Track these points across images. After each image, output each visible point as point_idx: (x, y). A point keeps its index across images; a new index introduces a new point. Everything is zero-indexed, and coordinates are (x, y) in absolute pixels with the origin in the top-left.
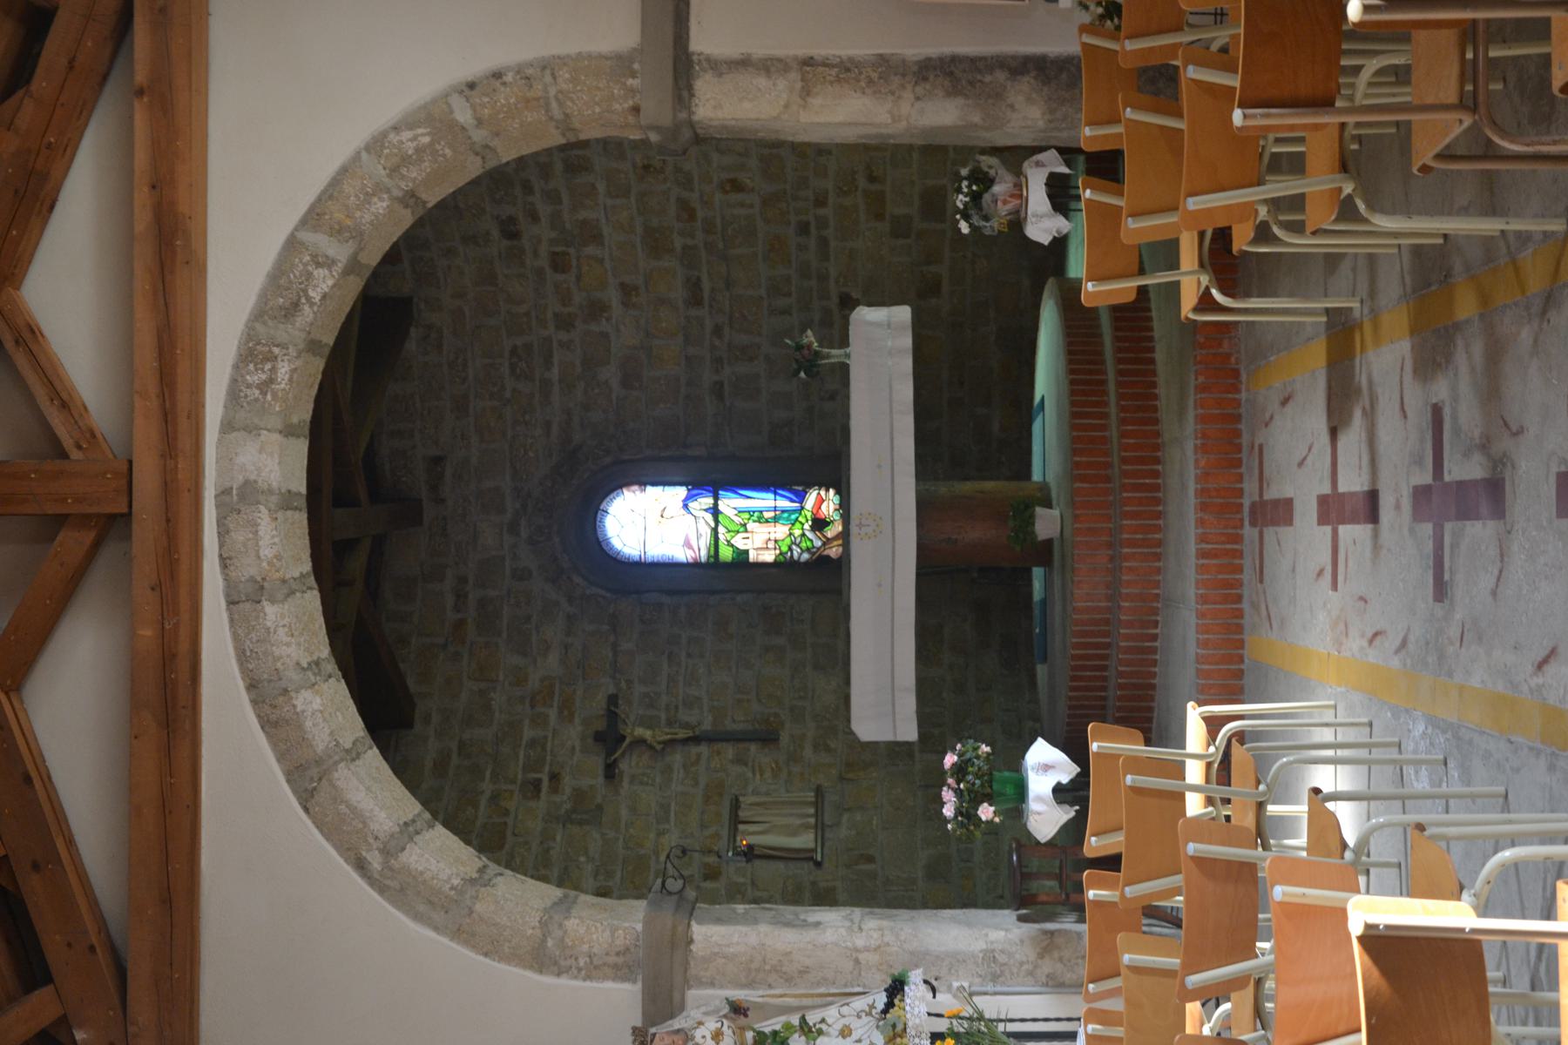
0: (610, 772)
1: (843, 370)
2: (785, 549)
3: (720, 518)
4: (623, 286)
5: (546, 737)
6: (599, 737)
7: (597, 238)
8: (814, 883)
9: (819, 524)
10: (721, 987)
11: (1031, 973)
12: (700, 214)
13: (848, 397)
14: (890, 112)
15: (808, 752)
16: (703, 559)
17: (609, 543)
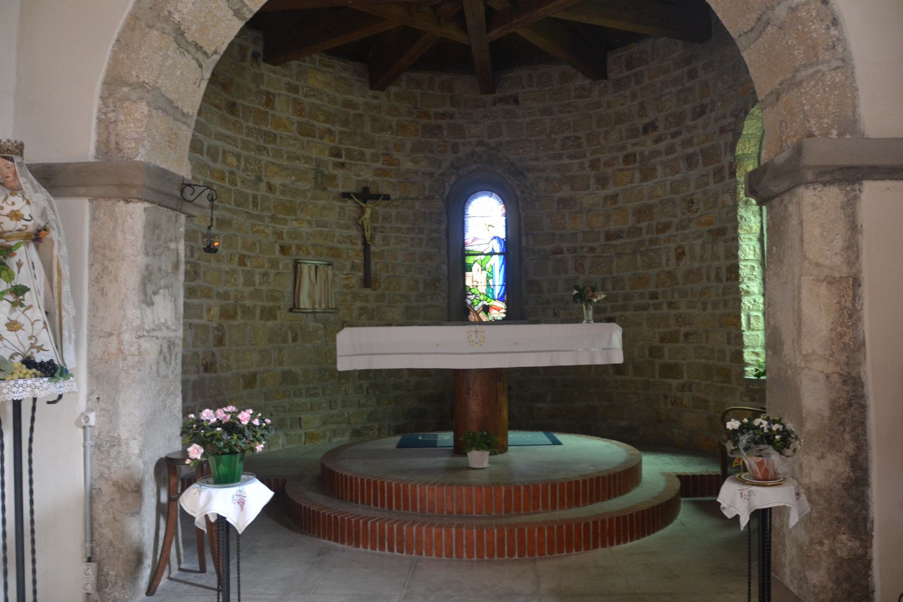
0: (346, 196)
1: (579, 320)
2: (473, 291)
3: (489, 257)
4: (617, 195)
5: (365, 161)
6: (366, 189)
7: (645, 178)
8: (279, 308)
9: (486, 309)
10: (91, 227)
11: (102, 475)
12: (662, 236)
13: (556, 323)
14: (814, 352)
15: (359, 304)
16: (467, 248)
17: (474, 198)
